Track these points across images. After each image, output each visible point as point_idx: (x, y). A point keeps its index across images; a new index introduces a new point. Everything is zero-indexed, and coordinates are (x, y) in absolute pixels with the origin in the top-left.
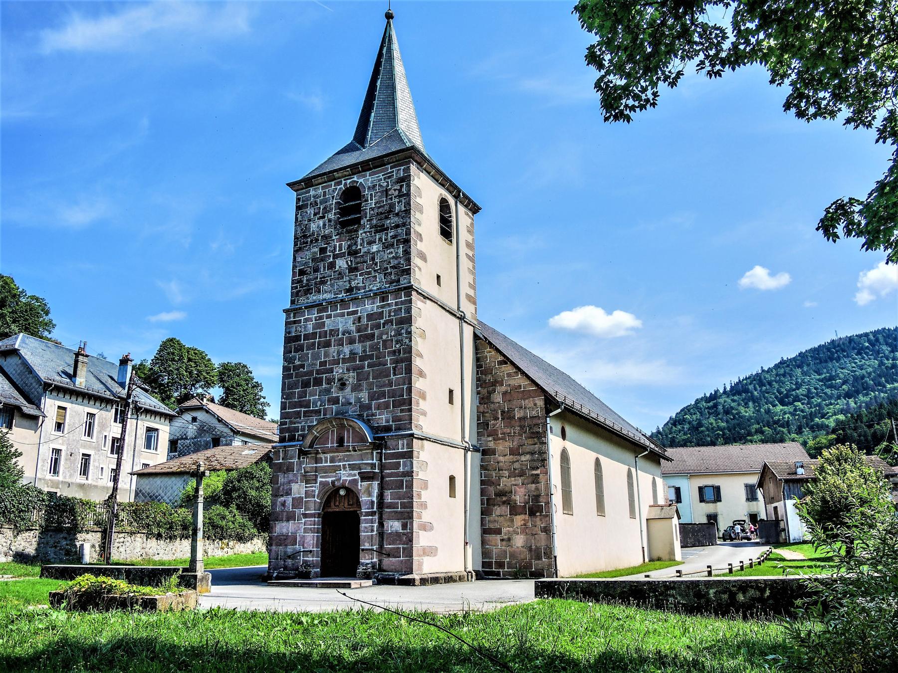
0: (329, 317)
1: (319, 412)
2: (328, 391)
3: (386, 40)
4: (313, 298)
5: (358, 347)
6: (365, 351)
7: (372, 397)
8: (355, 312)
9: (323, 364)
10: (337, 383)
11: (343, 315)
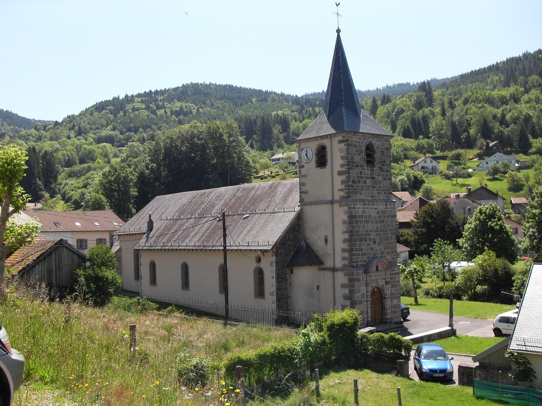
0: (367, 208)
1: (367, 254)
2: (369, 245)
3: (339, 38)
4: (359, 196)
5: (379, 225)
6: (381, 227)
7: (386, 248)
8: (376, 209)
9: (367, 231)
10: (372, 242)
11: (372, 209)
